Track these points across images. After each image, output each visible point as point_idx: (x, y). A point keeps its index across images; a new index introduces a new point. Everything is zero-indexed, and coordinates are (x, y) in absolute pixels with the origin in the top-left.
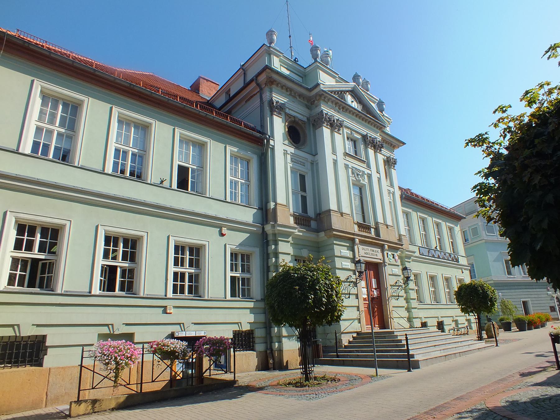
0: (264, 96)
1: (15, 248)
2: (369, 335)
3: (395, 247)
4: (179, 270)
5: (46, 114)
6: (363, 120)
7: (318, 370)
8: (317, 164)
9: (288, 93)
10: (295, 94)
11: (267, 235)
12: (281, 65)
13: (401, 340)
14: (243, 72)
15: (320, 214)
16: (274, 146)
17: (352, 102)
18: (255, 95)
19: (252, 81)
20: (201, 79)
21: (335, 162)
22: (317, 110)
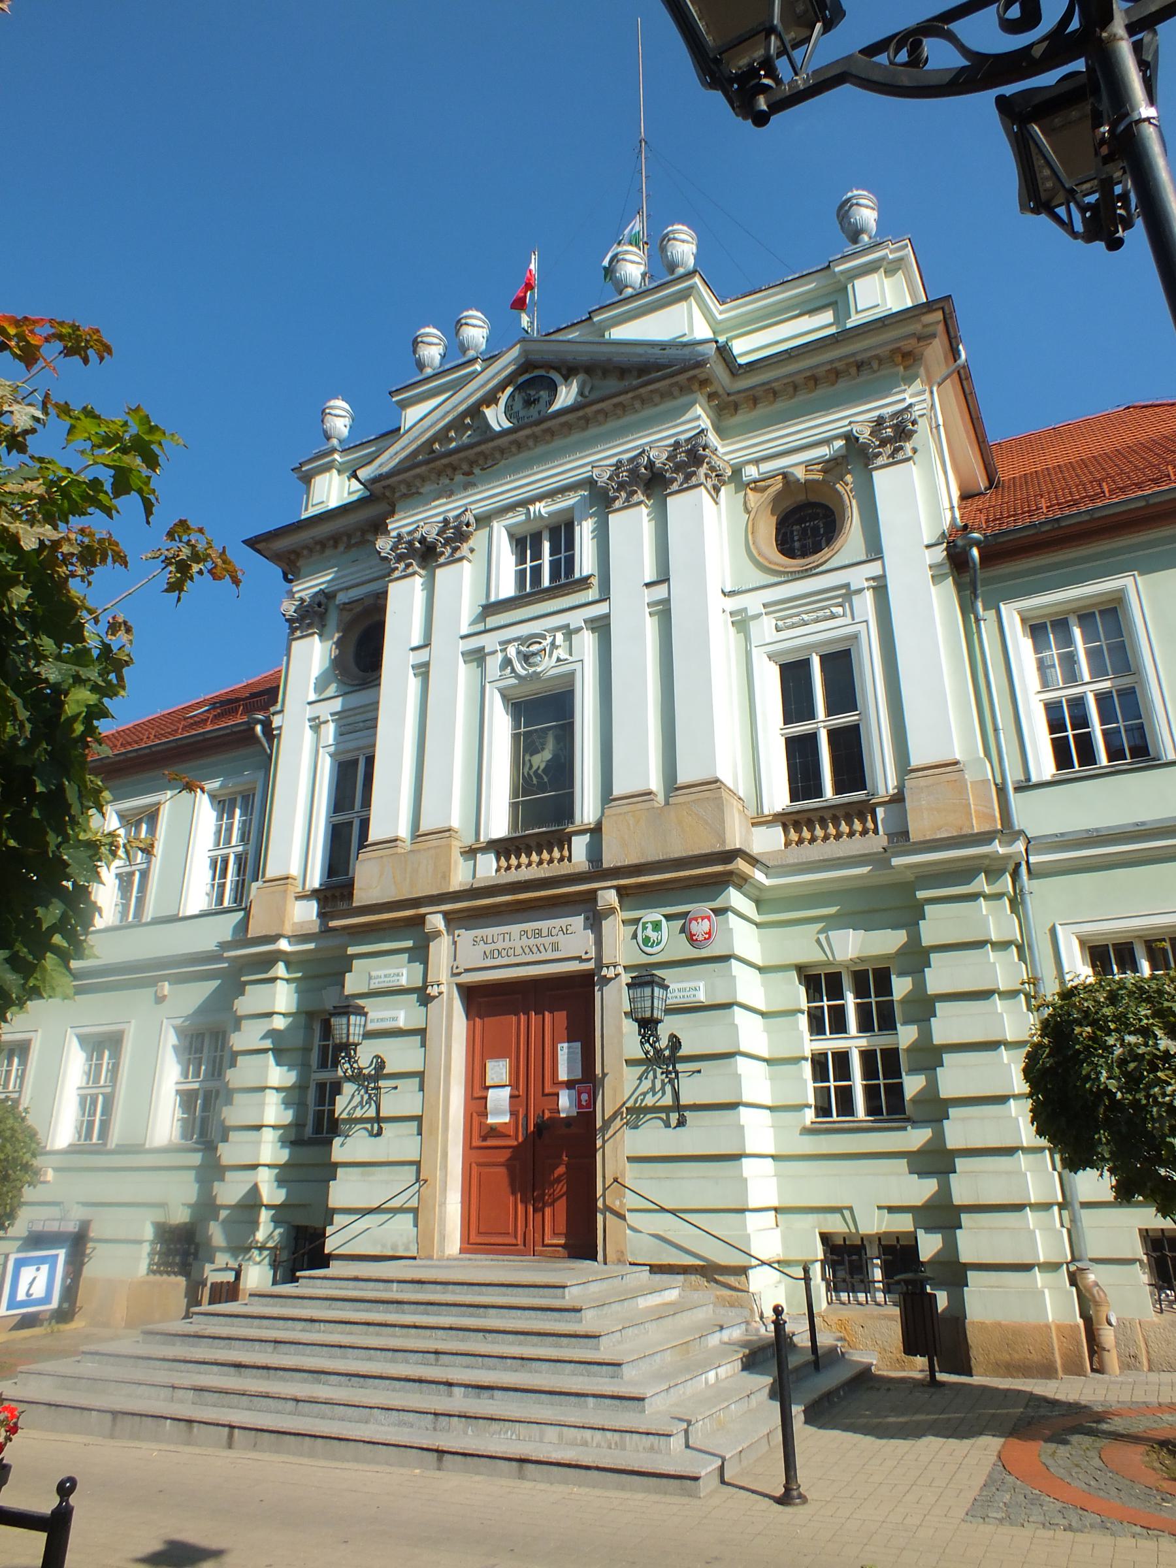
5: (1054, 666)
17: (539, 412)
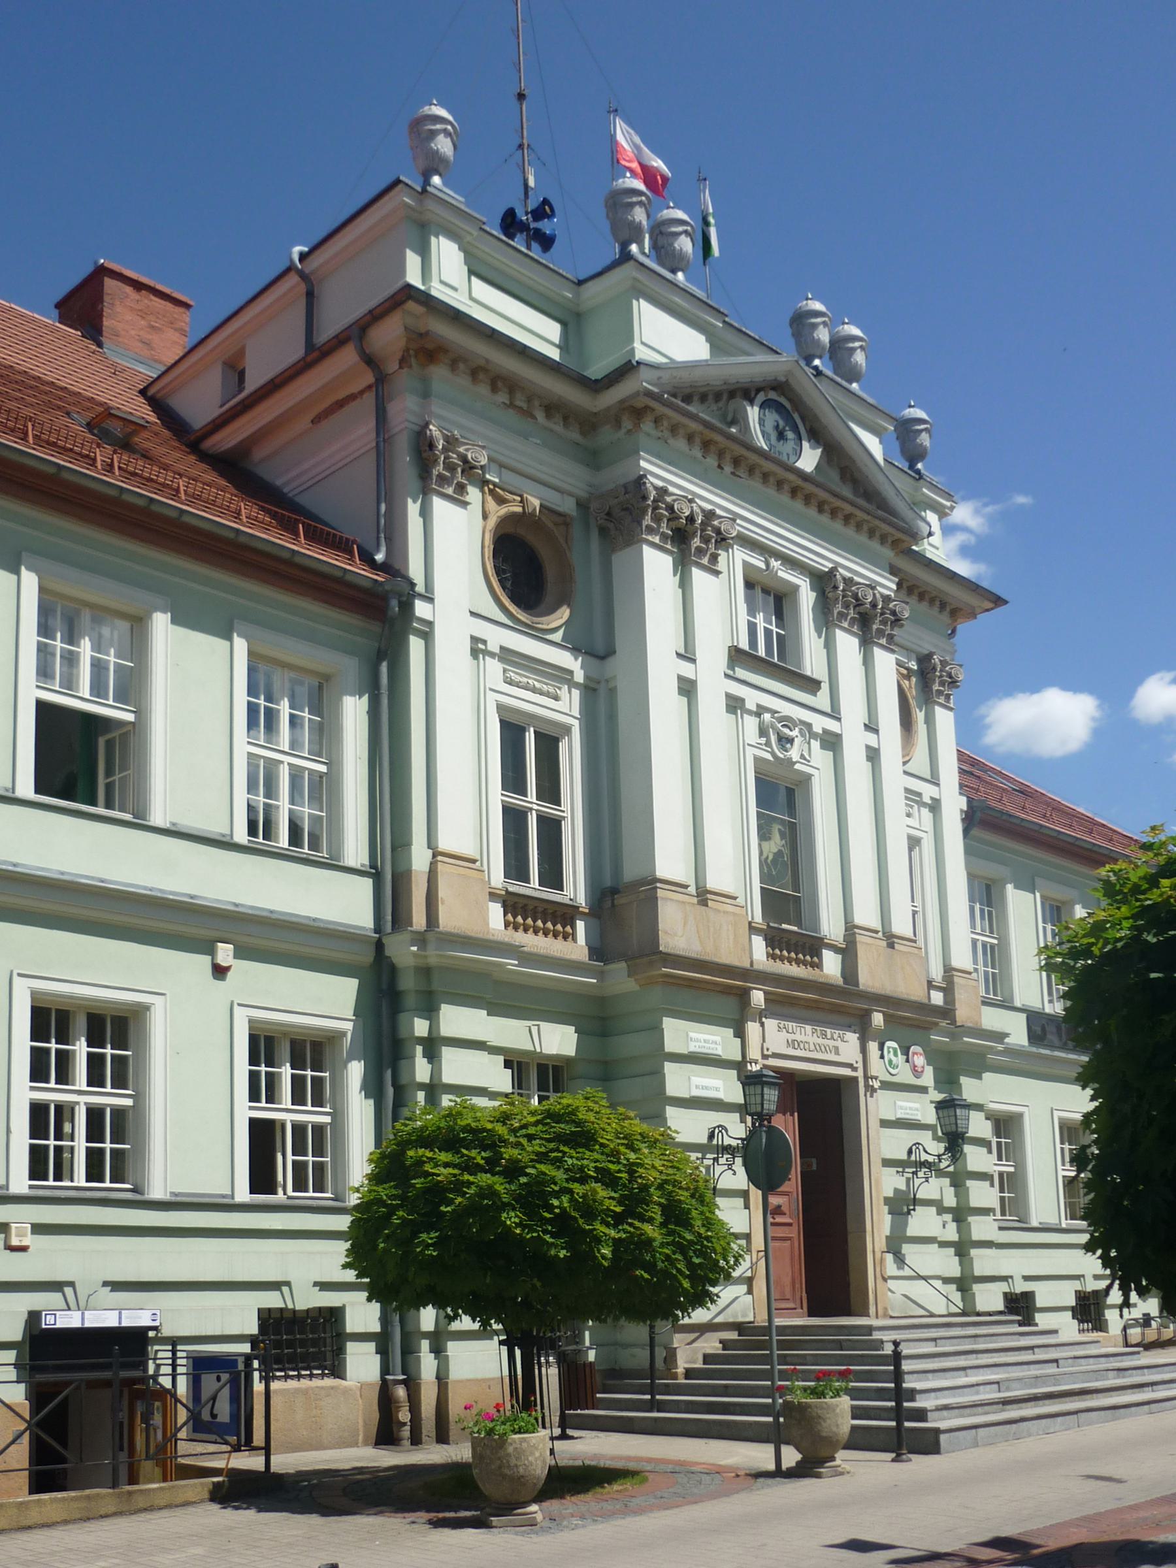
0: (393, 409)
1: (33, 1078)
2: (793, 1339)
3: (913, 1021)
4: (51, 1094)
6: (821, 510)
7: (570, 1432)
8: (612, 692)
9: (502, 397)
10: (529, 400)
11: (393, 970)
12: (471, 272)
13: (882, 1342)
14: (302, 288)
15: (614, 891)
16: (430, 624)
18: (352, 397)
19: (340, 341)
20: (109, 284)
21: (687, 688)
22: (615, 476)
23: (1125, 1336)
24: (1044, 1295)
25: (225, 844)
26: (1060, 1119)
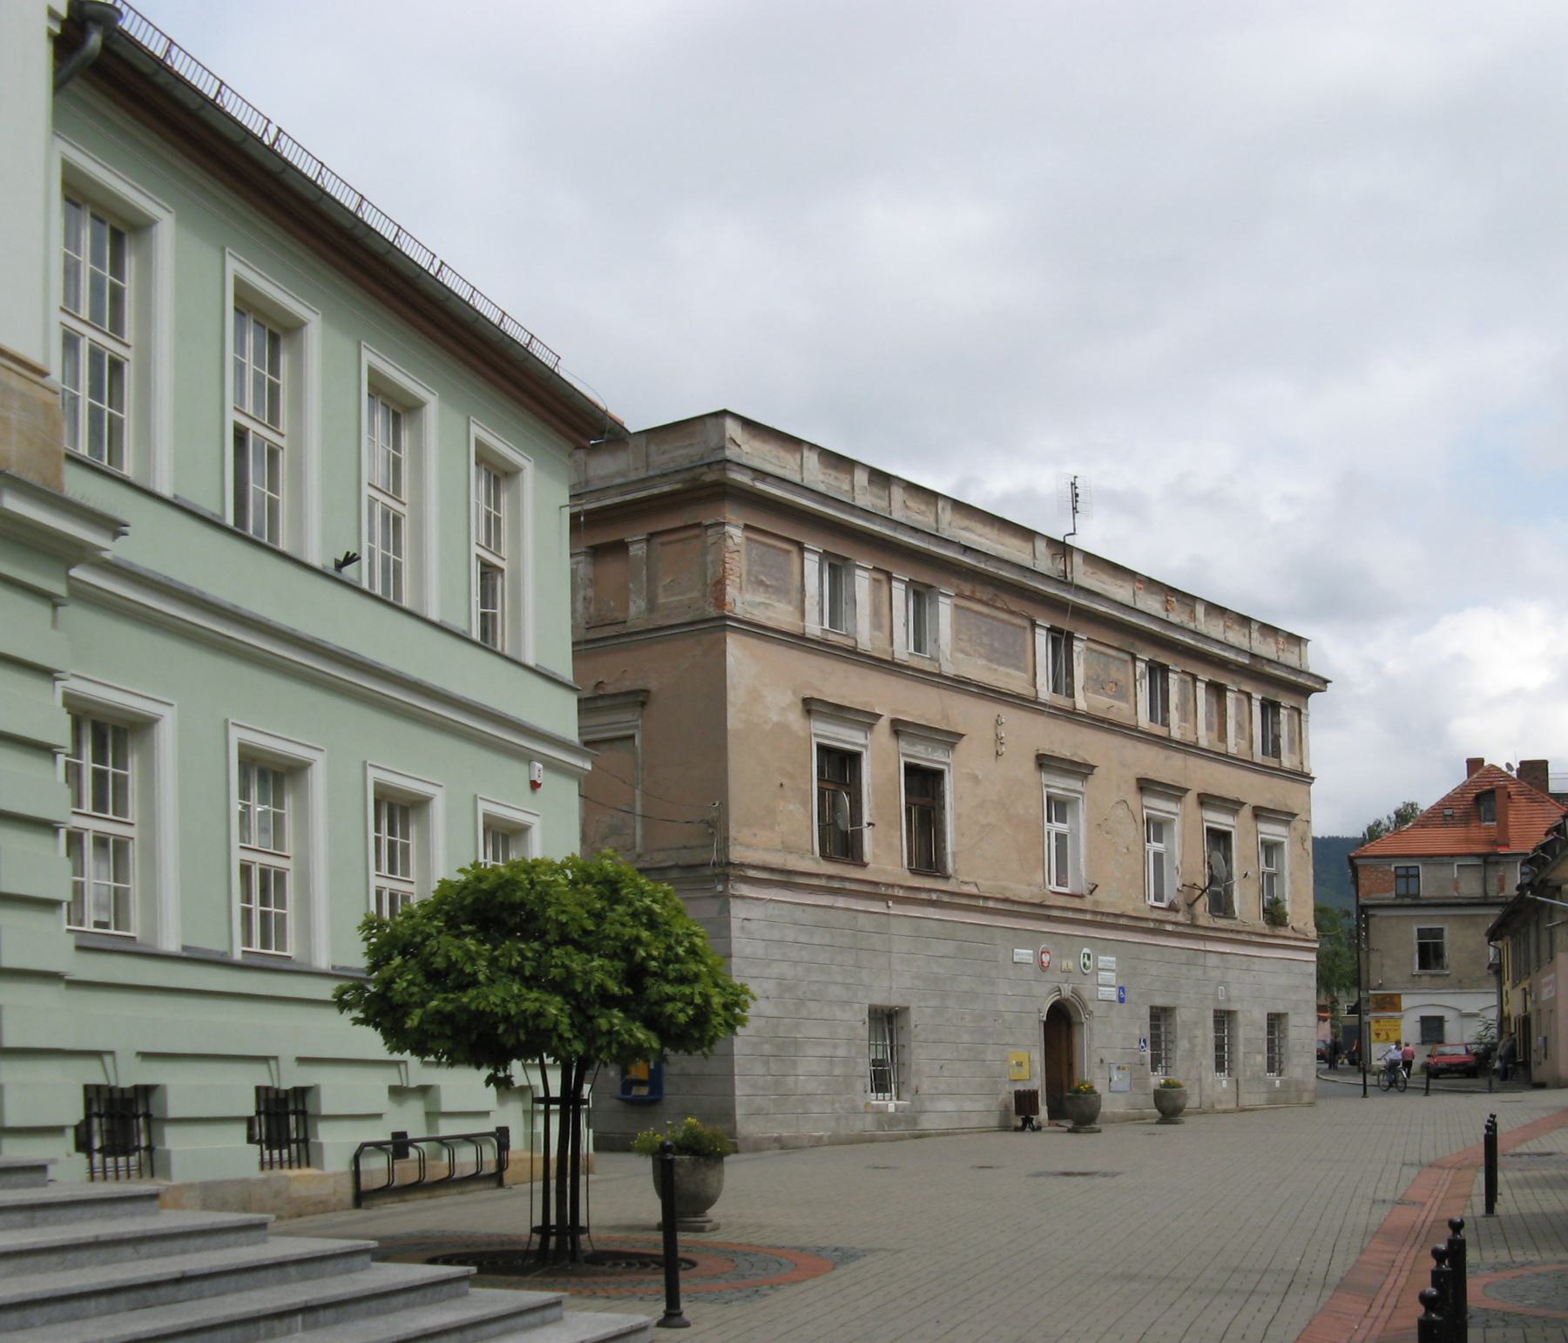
23: (357, 1174)
24: (183, 1090)
25: (216, 524)
26: (377, 785)
